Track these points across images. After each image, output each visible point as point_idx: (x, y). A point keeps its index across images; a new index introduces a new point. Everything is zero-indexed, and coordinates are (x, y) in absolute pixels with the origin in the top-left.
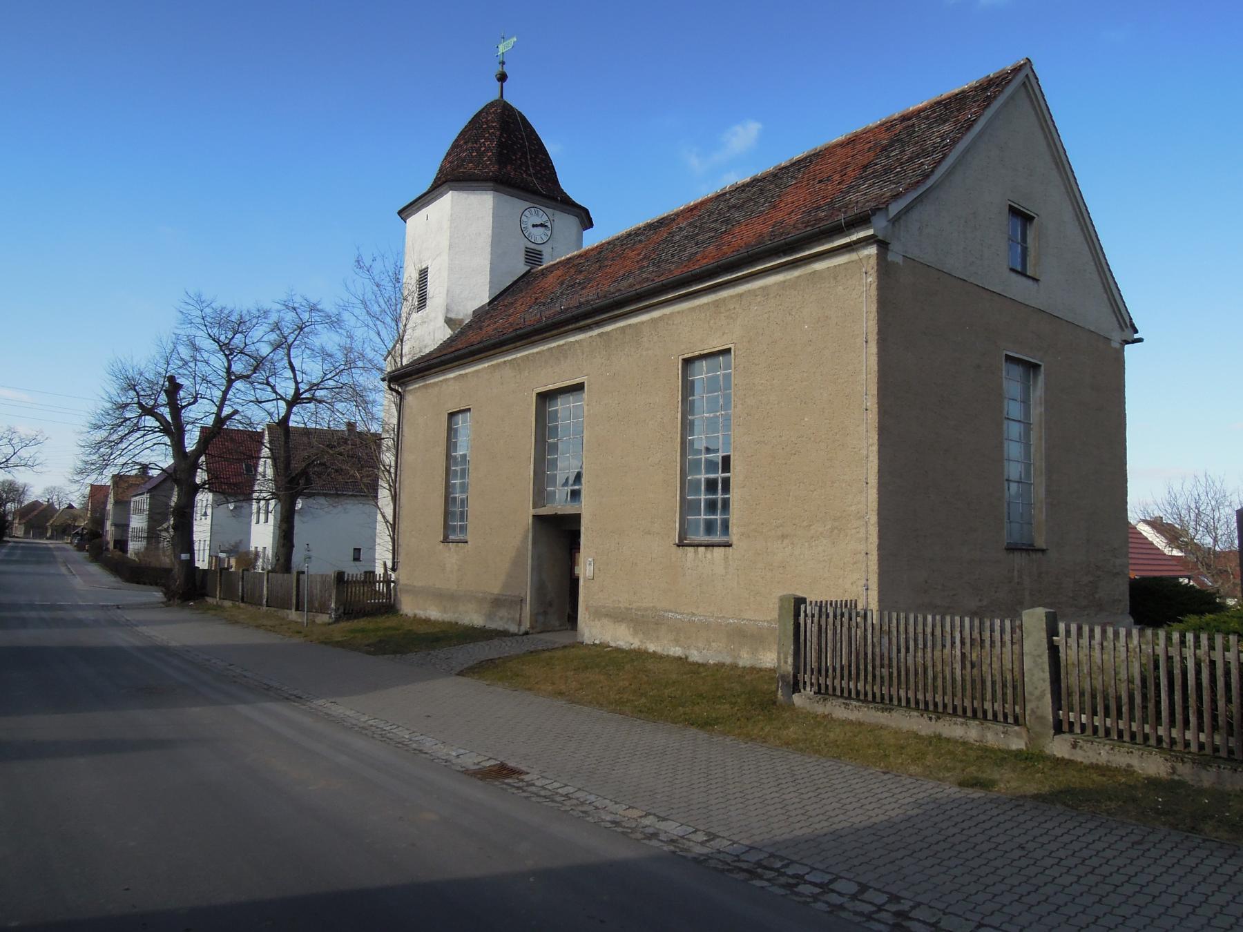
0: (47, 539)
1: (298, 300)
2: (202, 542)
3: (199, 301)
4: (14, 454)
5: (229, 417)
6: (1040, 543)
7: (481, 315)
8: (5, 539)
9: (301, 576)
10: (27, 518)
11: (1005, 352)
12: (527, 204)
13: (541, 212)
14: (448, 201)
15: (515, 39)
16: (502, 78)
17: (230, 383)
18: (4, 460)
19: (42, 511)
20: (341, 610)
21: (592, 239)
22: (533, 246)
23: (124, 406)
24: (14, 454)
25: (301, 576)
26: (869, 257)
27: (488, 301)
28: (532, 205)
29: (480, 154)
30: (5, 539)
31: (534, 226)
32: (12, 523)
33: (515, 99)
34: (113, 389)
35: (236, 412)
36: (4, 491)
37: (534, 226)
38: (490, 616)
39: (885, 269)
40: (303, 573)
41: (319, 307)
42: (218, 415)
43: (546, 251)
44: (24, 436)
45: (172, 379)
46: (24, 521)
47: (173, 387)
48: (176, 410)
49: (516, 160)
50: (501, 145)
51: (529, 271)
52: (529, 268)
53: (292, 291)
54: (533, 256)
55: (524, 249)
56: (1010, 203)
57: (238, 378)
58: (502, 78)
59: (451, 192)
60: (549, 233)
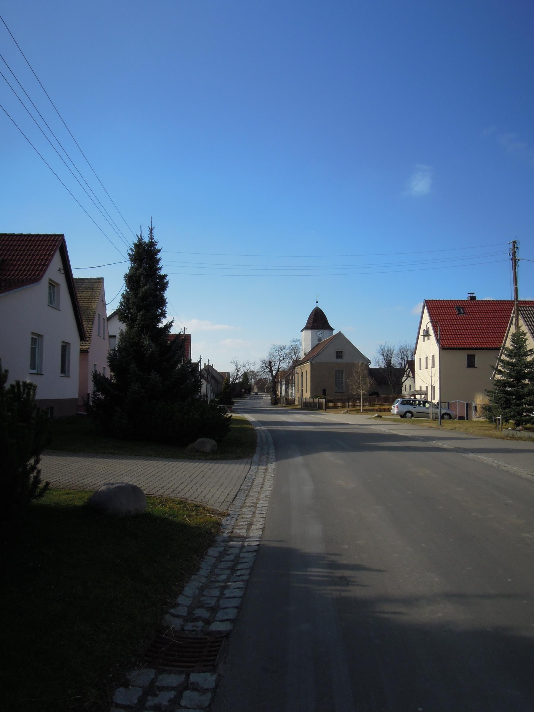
0: (265, 393)
1: (295, 340)
3: (273, 345)
5: (280, 369)
7: (309, 352)
8: (251, 393)
10: (258, 386)
12: (318, 331)
16: (317, 302)
18: (247, 370)
23: (262, 367)
26: (309, 364)
29: (310, 322)
30: (251, 393)
32: (254, 387)
33: (320, 307)
34: (261, 363)
38: (202, 392)
39: (311, 364)
41: (300, 340)
43: (322, 338)
45: (270, 361)
48: (271, 367)
54: (319, 340)
56: (470, 295)
58: (317, 302)
59: (304, 331)
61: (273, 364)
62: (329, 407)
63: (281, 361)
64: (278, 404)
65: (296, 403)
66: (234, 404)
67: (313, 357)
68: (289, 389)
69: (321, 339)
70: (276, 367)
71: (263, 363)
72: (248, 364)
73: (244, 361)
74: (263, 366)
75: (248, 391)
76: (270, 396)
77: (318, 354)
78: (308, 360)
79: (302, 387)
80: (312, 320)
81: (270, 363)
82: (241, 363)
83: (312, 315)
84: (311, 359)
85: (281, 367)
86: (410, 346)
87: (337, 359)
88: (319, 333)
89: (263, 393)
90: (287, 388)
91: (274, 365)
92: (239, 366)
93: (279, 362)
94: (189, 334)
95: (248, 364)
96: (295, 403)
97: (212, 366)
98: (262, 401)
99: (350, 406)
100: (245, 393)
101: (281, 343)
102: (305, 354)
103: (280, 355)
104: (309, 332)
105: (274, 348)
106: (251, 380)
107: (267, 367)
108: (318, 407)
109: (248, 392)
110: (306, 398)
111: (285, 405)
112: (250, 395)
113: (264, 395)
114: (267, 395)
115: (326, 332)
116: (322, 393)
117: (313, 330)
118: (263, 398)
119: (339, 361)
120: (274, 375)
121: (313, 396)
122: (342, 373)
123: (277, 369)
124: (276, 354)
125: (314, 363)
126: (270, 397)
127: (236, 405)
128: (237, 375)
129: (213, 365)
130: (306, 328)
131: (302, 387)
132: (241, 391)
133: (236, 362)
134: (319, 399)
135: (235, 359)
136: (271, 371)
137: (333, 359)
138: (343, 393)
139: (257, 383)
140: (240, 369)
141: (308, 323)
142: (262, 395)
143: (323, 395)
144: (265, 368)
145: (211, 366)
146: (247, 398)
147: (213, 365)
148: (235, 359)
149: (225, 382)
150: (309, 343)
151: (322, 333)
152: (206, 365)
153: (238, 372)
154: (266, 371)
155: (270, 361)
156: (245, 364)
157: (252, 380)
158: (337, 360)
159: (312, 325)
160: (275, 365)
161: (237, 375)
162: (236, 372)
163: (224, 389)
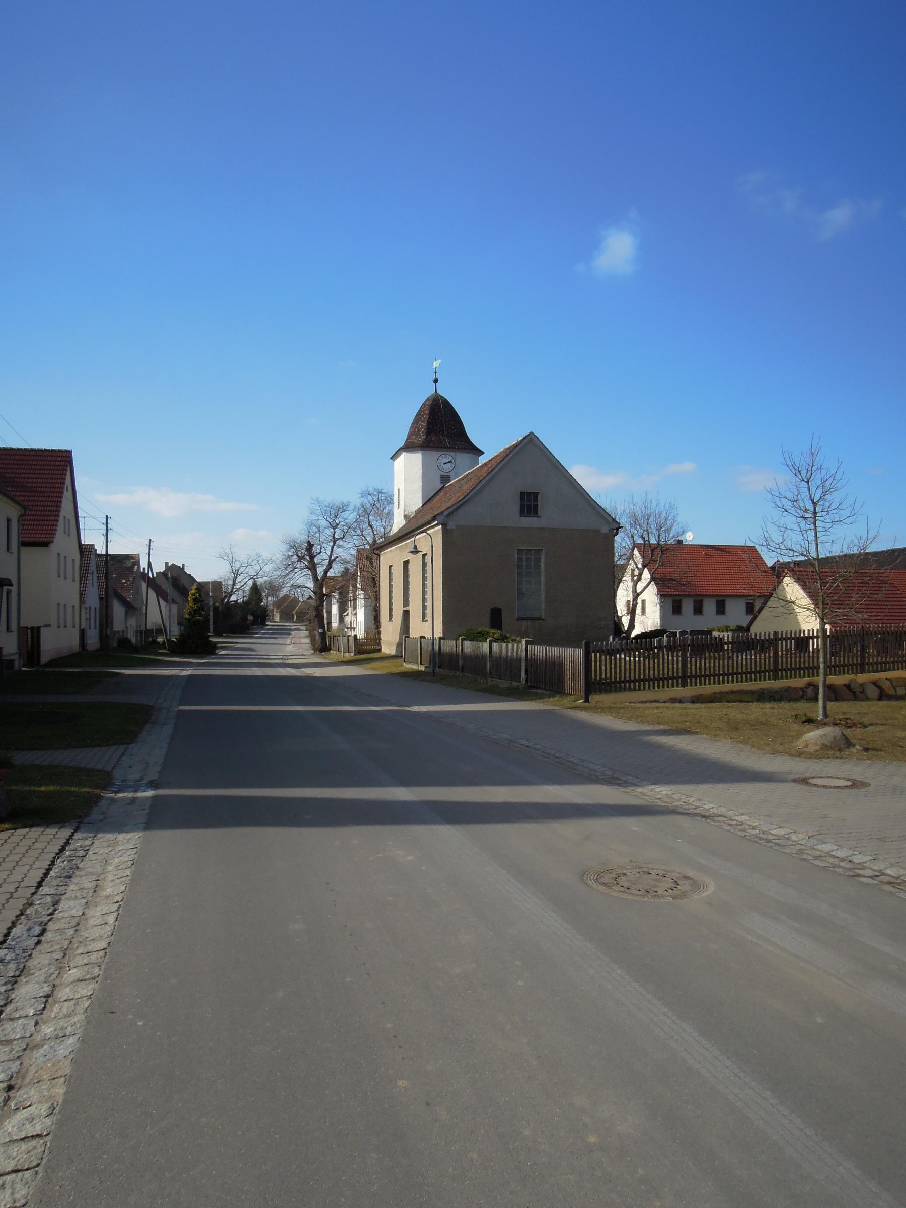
0: (294, 623)
2: (62, 624)
3: (317, 501)
4: (261, 569)
5: (334, 560)
6: (543, 618)
7: (419, 512)
9: (349, 637)
11: (517, 548)
12: (440, 453)
13: (448, 456)
14: (403, 456)
15: (440, 361)
16: (436, 381)
17: (335, 542)
18: (255, 574)
19: (291, 602)
20: (357, 651)
21: (483, 460)
22: (445, 474)
23: (290, 557)
24: (261, 569)
25: (349, 637)
27: (421, 505)
28: (442, 453)
29: (419, 430)
30: (267, 623)
31: (444, 464)
33: (445, 392)
34: (285, 547)
35: (337, 557)
36: (266, 588)
37: (444, 464)
38: (334, 614)
39: (445, 532)
40: (350, 636)
42: (330, 560)
43: (452, 475)
44: (265, 558)
45: (308, 542)
46: (279, 610)
47: (310, 546)
48: (312, 557)
49: (437, 429)
50: (429, 424)
51: (443, 487)
52: (443, 485)
53: (367, 485)
54: (445, 479)
55: (440, 476)
57: (338, 539)
60: (453, 465)
61: (316, 549)
62: (600, 683)
63: (338, 542)
64: (331, 650)
65: (383, 650)
66: (217, 652)
67: (449, 508)
68: (348, 614)
69: (449, 477)
70: (326, 557)
71: (291, 546)
72: (258, 561)
73: (248, 555)
74: (291, 554)
75: (259, 619)
76: (304, 628)
77: (468, 500)
78: (434, 519)
79: (406, 602)
80: (424, 424)
81: (310, 546)
82: (242, 555)
83: (424, 414)
84: (446, 513)
85: (337, 557)
86: (654, 504)
87: (521, 516)
88: (443, 459)
89: (290, 622)
90: (342, 610)
91: (318, 551)
92: (238, 565)
93: (332, 544)
94: (66, 451)
95: (258, 561)
96: (379, 650)
97: (181, 567)
98: (288, 641)
99: (690, 677)
100: (254, 623)
101: (336, 497)
102: (405, 516)
103: (333, 527)
104: (416, 458)
105: (318, 508)
106: (267, 598)
107: (301, 559)
108: (527, 681)
109: (259, 621)
110: (422, 637)
111: (352, 655)
112: (265, 627)
113: (293, 627)
114: (298, 627)
115: (462, 458)
116: (487, 618)
117: (424, 452)
118: (292, 632)
119: (528, 522)
120: (319, 578)
121: (579, 647)
122: (538, 560)
123: (326, 562)
124: (324, 523)
125: (454, 527)
126: (306, 630)
127: (223, 652)
128: (234, 584)
129: (183, 565)
130: (409, 447)
131: (406, 602)
132: (245, 619)
133: (230, 556)
134: (530, 647)
135: (228, 551)
136: (312, 567)
137: (511, 516)
138: (541, 621)
139: (279, 604)
140: (241, 570)
141: (413, 433)
142: (289, 627)
143: (492, 627)
144: (295, 558)
145: (179, 567)
146: (256, 633)
147: (183, 565)
148: (228, 551)
149: (192, 596)
150: (418, 486)
151: (451, 462)
152: (169, 565)
153: (236, 578)
154: (298, 566)
155: (308, 542)
156: (250, 561)
157: (270, 599)
158: (522, 518)
159: (423, 438)
160: (320, 552)
161: (234, 584)
162: (232, 578)
163: (190, 614)
